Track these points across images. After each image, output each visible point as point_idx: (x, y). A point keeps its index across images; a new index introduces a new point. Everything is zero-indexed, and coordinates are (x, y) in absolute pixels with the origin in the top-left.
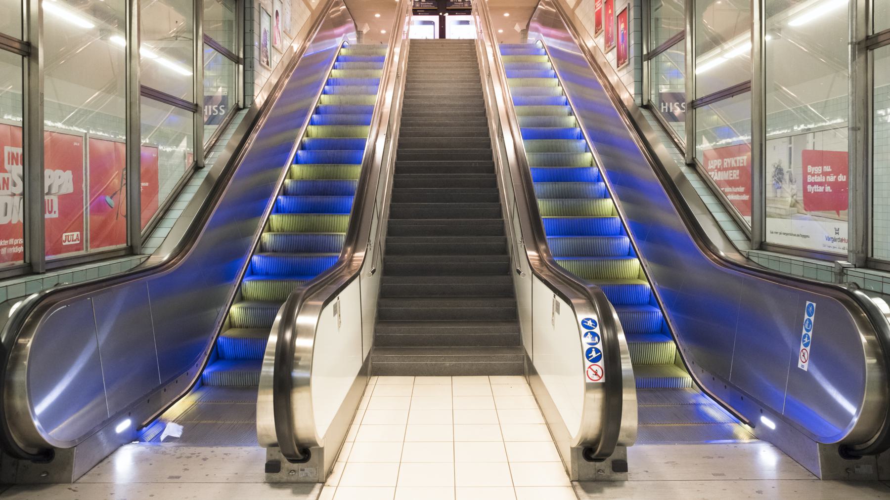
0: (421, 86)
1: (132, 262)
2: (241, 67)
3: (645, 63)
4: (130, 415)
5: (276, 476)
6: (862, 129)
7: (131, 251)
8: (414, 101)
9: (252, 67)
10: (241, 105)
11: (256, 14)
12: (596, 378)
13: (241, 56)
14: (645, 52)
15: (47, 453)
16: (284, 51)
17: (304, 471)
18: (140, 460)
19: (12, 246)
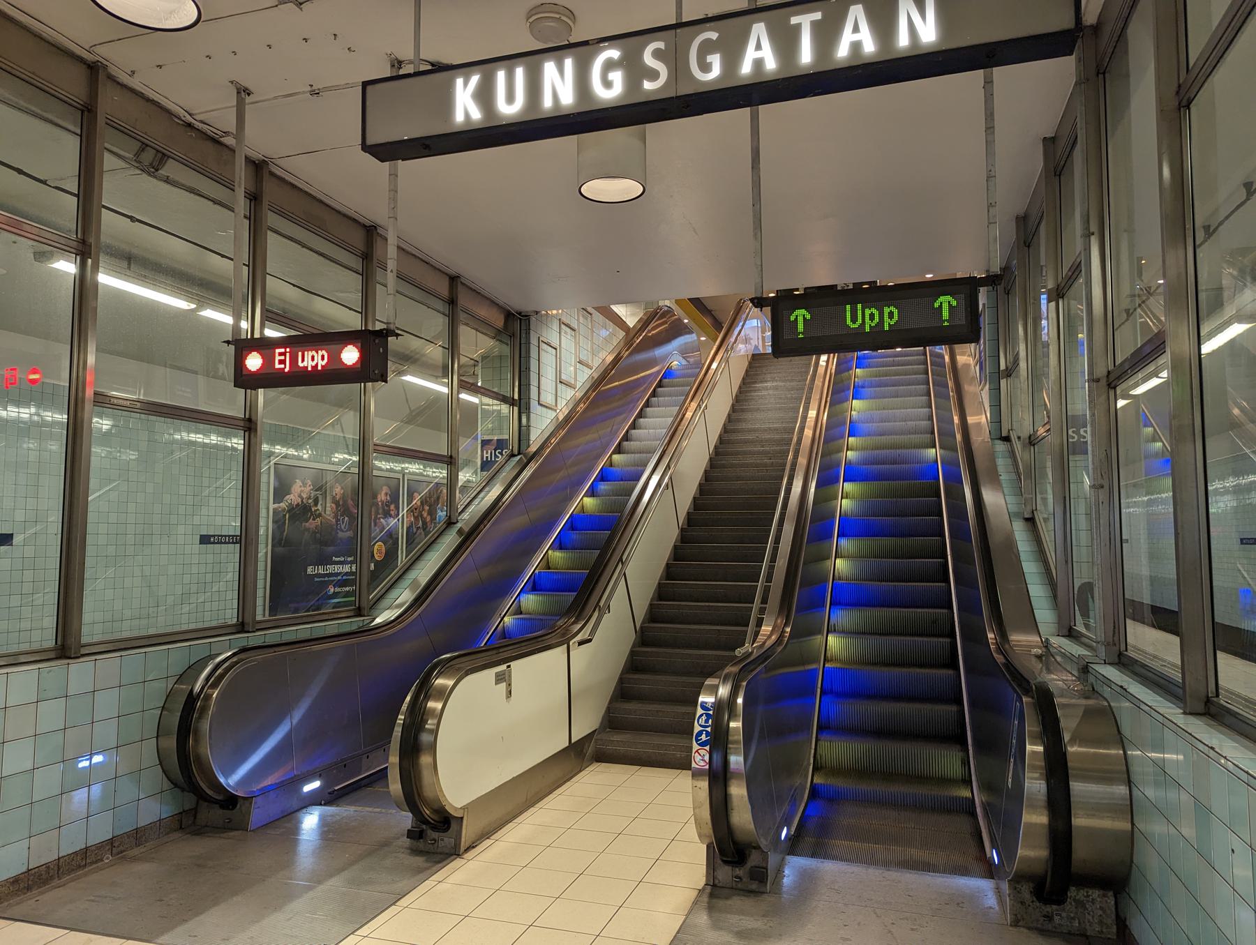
0: (758, 415)
1: (354, 623)
2: (516, 409)
3: (1003, 382)
4: (320, 776)
5: (421, 844)
6: (1107, 487)
7: (359, 612)
8: (733, 437)
9: (528, 408)
10: (516, 452)
11: (534, 354)
12: (702, 763)
13: (516, 397)
14: (1003, 367)
15: (230, 801)
16: (579, 385)
17: (446, 840)
18: (324, 823)
19: (767, 590)
